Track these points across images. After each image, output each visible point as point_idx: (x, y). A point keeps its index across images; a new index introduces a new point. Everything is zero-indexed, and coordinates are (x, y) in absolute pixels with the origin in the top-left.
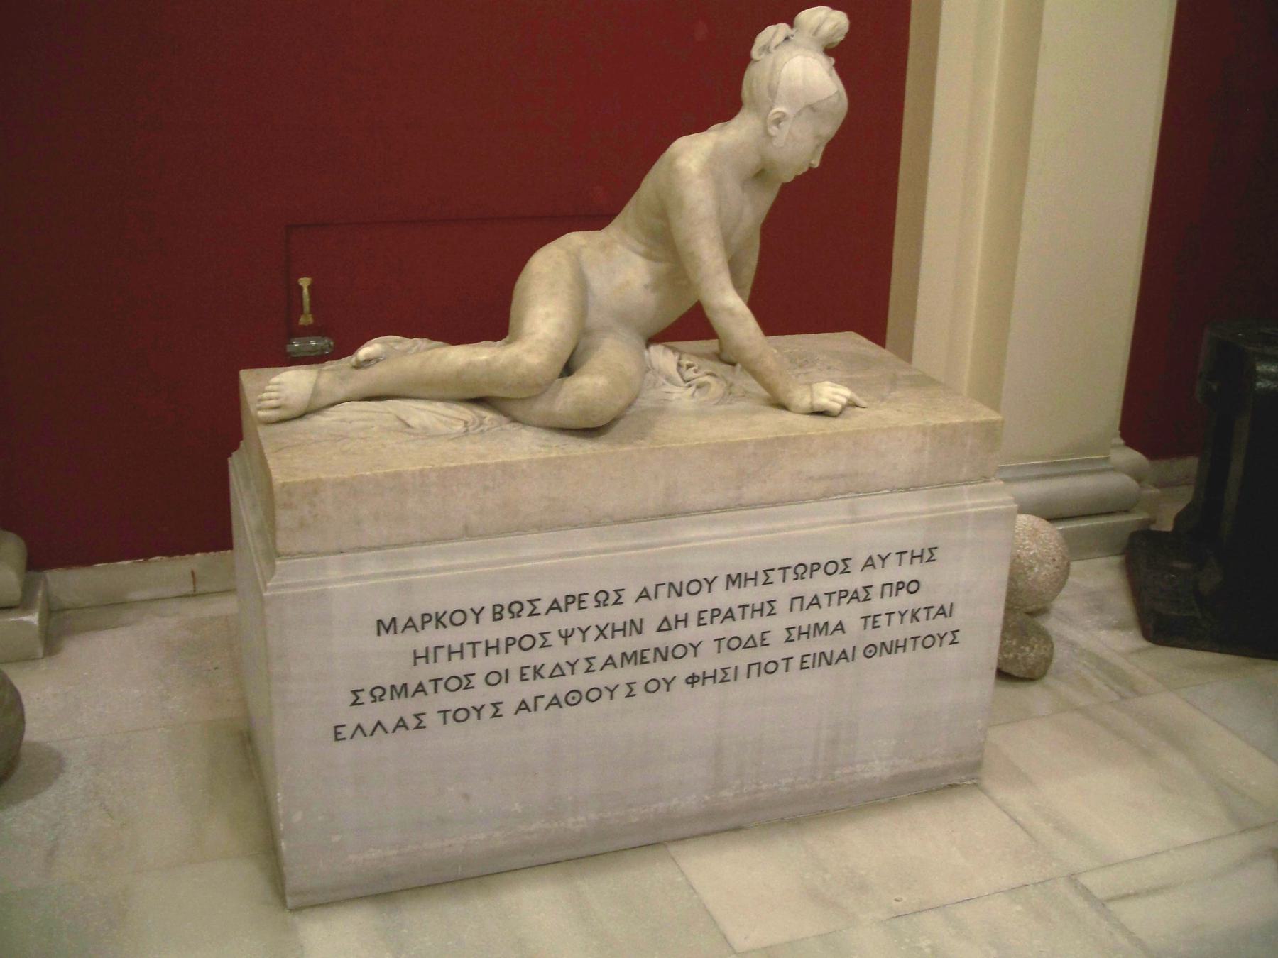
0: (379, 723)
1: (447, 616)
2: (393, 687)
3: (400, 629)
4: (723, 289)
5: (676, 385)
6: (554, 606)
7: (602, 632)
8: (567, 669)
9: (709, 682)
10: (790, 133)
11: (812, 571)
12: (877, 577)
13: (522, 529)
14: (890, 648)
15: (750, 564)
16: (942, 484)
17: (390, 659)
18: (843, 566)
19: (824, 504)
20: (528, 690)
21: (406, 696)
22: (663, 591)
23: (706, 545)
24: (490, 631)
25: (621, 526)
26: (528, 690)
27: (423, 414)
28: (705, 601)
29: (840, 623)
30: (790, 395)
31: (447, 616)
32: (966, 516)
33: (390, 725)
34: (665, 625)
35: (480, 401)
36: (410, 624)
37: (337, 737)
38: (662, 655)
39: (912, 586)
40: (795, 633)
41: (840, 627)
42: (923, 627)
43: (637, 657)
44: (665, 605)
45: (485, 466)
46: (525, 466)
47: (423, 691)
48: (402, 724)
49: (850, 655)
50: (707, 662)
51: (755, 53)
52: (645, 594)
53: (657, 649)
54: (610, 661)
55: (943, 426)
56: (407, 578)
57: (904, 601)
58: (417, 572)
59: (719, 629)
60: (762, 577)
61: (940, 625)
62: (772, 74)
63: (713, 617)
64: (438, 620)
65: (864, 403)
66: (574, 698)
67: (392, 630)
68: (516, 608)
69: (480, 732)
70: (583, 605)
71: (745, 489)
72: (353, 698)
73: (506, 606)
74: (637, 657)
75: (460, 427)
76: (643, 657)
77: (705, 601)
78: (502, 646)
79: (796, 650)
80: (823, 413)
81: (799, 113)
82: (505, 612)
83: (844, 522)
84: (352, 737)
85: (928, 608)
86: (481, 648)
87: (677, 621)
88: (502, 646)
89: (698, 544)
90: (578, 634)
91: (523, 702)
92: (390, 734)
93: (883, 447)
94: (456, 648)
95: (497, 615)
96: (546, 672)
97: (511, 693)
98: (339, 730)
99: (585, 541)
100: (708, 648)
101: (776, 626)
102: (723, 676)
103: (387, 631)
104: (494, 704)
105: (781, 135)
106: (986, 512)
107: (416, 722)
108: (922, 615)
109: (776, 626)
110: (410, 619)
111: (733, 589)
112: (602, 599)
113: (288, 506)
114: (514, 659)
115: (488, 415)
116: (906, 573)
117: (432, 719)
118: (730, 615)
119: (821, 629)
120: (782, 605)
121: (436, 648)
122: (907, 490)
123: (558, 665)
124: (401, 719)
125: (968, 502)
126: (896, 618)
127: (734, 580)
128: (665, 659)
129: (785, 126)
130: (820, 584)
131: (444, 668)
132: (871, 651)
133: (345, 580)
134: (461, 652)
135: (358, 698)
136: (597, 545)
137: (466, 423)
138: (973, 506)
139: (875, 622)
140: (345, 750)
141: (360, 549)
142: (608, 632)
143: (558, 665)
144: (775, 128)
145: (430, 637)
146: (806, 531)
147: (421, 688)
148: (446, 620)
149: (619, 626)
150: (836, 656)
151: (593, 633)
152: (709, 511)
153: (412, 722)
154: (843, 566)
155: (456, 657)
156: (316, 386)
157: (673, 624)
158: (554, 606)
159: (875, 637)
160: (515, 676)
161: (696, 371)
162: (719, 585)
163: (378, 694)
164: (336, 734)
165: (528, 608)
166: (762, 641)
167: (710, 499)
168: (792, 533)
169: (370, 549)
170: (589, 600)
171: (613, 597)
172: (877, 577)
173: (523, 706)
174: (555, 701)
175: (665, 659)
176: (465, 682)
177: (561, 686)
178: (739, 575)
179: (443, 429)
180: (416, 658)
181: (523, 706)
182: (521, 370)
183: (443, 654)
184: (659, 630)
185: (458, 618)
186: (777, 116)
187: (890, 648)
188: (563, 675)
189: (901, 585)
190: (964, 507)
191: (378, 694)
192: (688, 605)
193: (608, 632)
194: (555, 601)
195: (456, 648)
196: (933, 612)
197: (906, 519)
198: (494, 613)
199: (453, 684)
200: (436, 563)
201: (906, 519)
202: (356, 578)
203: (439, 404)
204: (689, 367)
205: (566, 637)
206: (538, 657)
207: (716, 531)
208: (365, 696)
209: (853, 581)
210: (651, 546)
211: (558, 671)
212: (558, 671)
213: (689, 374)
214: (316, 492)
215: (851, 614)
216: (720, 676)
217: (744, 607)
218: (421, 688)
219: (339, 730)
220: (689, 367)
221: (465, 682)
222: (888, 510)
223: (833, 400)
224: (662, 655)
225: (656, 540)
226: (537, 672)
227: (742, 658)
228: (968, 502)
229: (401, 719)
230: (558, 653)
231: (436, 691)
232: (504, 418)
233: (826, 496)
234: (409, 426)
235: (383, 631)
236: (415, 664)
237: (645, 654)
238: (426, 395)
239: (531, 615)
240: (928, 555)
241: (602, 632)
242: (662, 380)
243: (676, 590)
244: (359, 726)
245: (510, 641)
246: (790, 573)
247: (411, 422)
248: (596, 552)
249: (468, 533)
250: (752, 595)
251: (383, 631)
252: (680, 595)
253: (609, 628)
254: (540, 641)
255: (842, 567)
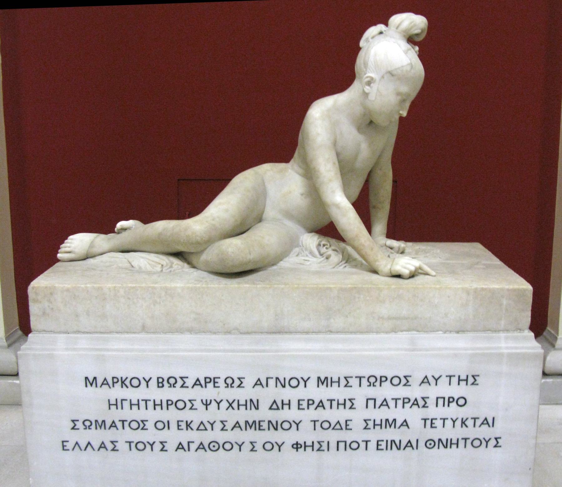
0: (89, 443)
1: (128, 380)
2: (96, 421)
3: (99, 385)
4: (333, 192)
5: (314, 256)
6: (197, 383)
7: (230, 405)
8: (209, 426)
9: (309, 449)
10: (378, 90)
11: (381, 381)
12: (432, 392)
13: (180, 331)
14: (448, 444)
15: (334, 372)
16: (485, 330)
17: (93, 404)
18: (406, 381)
19: (392, 335)
20: (185, 436)
21: (105, 428)
22: (272, 382)
23: (302, 354)
24: (154, 393)
25: (244, 336)
26: (185, 436)
27: (142, 260)
28: (301, 393)
29: (405, 421)
30: (377, 263)
31: (128, 380)
32: (501, 355)
33: (96, 445)
34: (274, 406)
35: (178, 255)
36: (105, 382)
37: (64, 448)
38: (275, 426)
39: (461, 402)
40: (371, 424)
41: (405, 423)
42: (471, 432)
43: (256, 425)
44: (273, 393)
45: (154, 288)
46: (180, 291)
47: (116, 426)
48: (103, 446)
49: (414, 445)
50: (306, 435)
51: (362, 43)
52: (258, 383)
53: (270, 422)
54: (237, 425)
55: (483, 289)
56: (102, 353)
57: (453, 411)
58: (108, 350)
59: (312, 413)
60: (343, 382)
61: (484, 432)
62: (366, 54)
63: (308, 405)
64: (123, 382)
65: (433, 273)
66: (214, 446)
67: (94, 384)
68: (172, 381)
69: (151, 458)
70: (216, 385)
71: (332, 320)
72: (72, 425)
73: (166, 380)
74: (256, 425)
75: (159, 268)
76: (260, 426)
77: (301, 393)
78: (164, 404)
79: (374, 435)
80: (399, 276)
81: (383, 77)
82: (165, 383)
83: (406, 350)
84: (73, 449)
85: (475, 419)
86: (150, 404)
87: (283, 404)
88: (164, 404)
89: (295, 353)
90: (214, 404)
91: (180, 444)
92: (83, 451)
93: (436, 301)
94: (135, 401)
95: (160, 383)
96: (194, 426)
97: (173, 437)
98: (65, 444)
99: (219, 342)
100: (307, 426)
101: (357, 416)
102: (319, 447)
103: (91, 385)
104: (161, 443)
105: (372, 90)
106: (518, 354)
107: (112, 446)
108: (470, 423)
109: (357, 416)
110: (105, 379)
111: (323, 387)
112: (230, 383)
113: (36, 301)
114: (172, 415)
115: (176, 262)
116: (456, 391)
117: (122, 446)
118: (321, 404)
119: (390, 423)
120: (360, 403)
121: (122, 400)
122: (458, 332)
123: (202, 423)
124: (103, 443)
125: (503, 345)
126: (449, 423)
127: (322, 381)
128: (276, 429)
129: (374, 86)
130: (387, 391)
131: (128, 414)
132: (430, 444)
133: (67, 349)
134: (138, 405)
135: (75, 425)
136: (227, 347)
137: (162, 265)
138: (507, 348)
139: (432, 423)
140: (69, 456)
141: (78, 332)
142: (235, 405)
143: (202, 423)
144: (367, 87)
145: (118, 392)
146: (373, 353)
147: (113, 425)
148: (127, 382)
149: (242, 402)
150: (403, 444)
151: (224, 405)
152: (307, 333)
153: (110, 446)
154: (406, 381)
155: (135, 408)
156: (92, 242)
157: (280, 405)
158: (197, 383)
159: (435, 434)
160: (173, 425)
161: (327, 248)
162: (312, 383)
163: (88, 424)
164: (63, 446)
165: (180, 382)
166: (347, 426)
167: (306, 325)
168: (354, 353)
169: (84, 333)
170: (221, 382)
171: (237, 382)
172: (432, 392)
173: (180, 447)
174: (201, 446)
175: (440, 440)
176: (142, 425)
177: (207, 437)
178: (326, 378)
179: (149, 268)
180: (110, 405)
181: (180, 447)
182: (189, 233)
183: (126, 404)
184: (270, 408)
185: (135, 382)
186: (368, 79)
187: (448, 444)
188: (206, 429)
189: (451, 400)
190: (500, 348)
191: (88, 424)
192: (287, 394)
193: (235, 405)
194: (198, 380)
195: (135, 401)
196: (478, 422)
197: (452, 352)
198: (158, 383)
199: (134, 425)
200: (122, 346)
201: (452, 352)
202: (75, 349)
203: (153, 255)
204: (324, 245)
205: (207, 405)
206: (187, 415)
207: (309, 346)
208: (79, 425)
209: (415, 392)
210: (264, 351)
211: (202, 427)
212: (202, 427)
213: (323, 250)
214: (51, 294)
215: (414, 416)
216: (316, 446)
217: (331, 401)
218: (113, 425)
219: (65, 444)
220: (324, 245)
221: (142, 425)
222: (440, 344)
223: (405, 268)
224: (275, 426)
225: (267, 348)
226: (188, 425)
227: (333, 436)
228: (503, 345)
229: (103, 443)
230: (199, 415)
231: (123, 428)
232: (186, 265)
233: (394, 330)
234: (133, 267)
235: (88, 384)
236: (110, 409)
237: (262, 423)
238: (149, 250)
239: (182, 386)
240: (472, 380)
241: (230, 405)
242: (307, 253)
243: (282, 383)
244: (77, 443)
245: (169, 403)
246: (364, 381)
247: (133, 264)
248: (225, 351)
249: (144, 329)
250: (337, 393)
251: (88, 384)
252: (284, 386)
253: (236, 402)
254: (189, 405)
255: (404, 381)
